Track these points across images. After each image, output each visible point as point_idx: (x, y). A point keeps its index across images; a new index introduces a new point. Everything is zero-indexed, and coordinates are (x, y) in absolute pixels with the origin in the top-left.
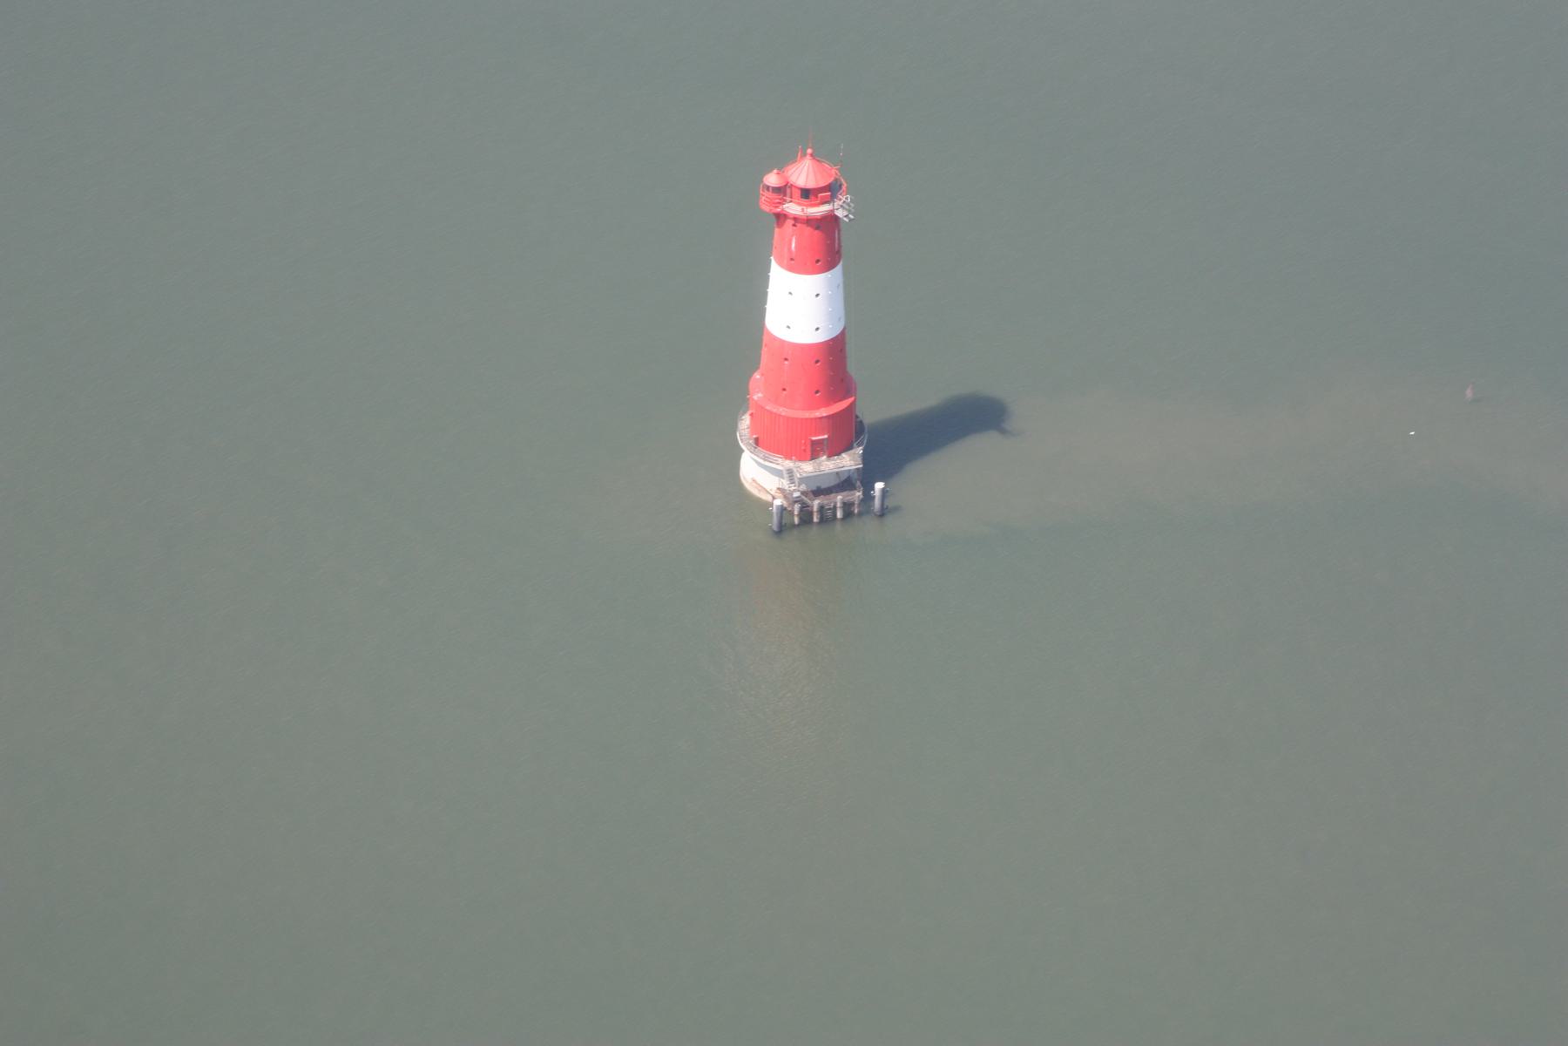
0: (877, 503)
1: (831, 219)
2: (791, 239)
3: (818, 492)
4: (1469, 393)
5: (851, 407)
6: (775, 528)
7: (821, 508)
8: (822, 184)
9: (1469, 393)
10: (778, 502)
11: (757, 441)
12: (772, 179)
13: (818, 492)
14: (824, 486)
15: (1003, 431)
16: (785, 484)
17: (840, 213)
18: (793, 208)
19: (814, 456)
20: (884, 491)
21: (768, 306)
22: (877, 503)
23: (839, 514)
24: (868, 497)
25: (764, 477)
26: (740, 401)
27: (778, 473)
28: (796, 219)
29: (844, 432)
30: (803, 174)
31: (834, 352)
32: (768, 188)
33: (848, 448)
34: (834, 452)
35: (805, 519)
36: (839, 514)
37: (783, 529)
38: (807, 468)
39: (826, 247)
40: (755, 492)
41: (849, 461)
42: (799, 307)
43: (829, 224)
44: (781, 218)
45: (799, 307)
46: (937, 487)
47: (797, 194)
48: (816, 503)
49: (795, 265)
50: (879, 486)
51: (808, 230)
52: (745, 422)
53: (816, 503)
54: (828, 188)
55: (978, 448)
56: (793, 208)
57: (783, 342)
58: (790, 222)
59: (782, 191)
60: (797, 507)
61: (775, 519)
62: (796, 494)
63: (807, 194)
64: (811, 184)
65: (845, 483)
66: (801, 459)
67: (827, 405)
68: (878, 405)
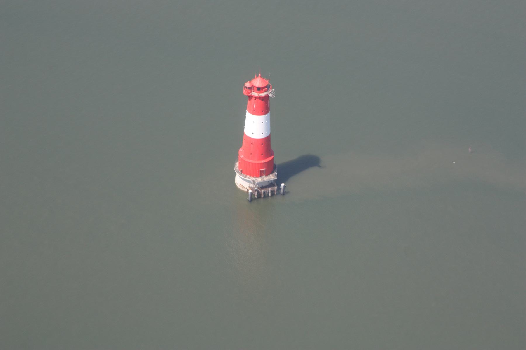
0: (282, 190)
1: (267, 97)
2: (254, 104)
3: (262, 188)
4: (470, 150)
7: (264, 193)
8: (264, 86)
9: (470, 150)
10: (250, 191)
11: (242, 171)
12: (248, 85)
13: (262, 188)
14: (264, 185)
15: (319, 166)
16: (252, 185)
17: (270, 95)
19: (261, 176)
20: (284, 187)
22: (282, 190)
23: (270, 195)
24: (279, 188)
25: (243, 183)
26: (236, 158)
27: (250, 182)
28: (256, 97)
29: (270, 168)
30: (258, 82)
31: (267, 141)
32: (246, 87)
33: (272, 172)
35: (258, 197)
36: (270, 195)
37: (252, 200)
38: (259, 180)
39: (265, 107)
40: (241, 188)
41: (272, 177)
42: (255, 126)
44: (250, 97)
45: (255, 126)
46: (301, 184)
47: (256, 89)
48: (263, 191)
49: (255, 112)
50: (283, 185)
51: (260, 101)
52: (237, 165)
53: (263, 191)
56: (255, 94)
57: (251, 138)
59: (251, 88)
60: (256, 193)
61: (249, 197)
62: (256, 188)
63: (259, 89)
64: (261, 86)
66: (257, 177)
67: (265, 158)
68: (278, 161)
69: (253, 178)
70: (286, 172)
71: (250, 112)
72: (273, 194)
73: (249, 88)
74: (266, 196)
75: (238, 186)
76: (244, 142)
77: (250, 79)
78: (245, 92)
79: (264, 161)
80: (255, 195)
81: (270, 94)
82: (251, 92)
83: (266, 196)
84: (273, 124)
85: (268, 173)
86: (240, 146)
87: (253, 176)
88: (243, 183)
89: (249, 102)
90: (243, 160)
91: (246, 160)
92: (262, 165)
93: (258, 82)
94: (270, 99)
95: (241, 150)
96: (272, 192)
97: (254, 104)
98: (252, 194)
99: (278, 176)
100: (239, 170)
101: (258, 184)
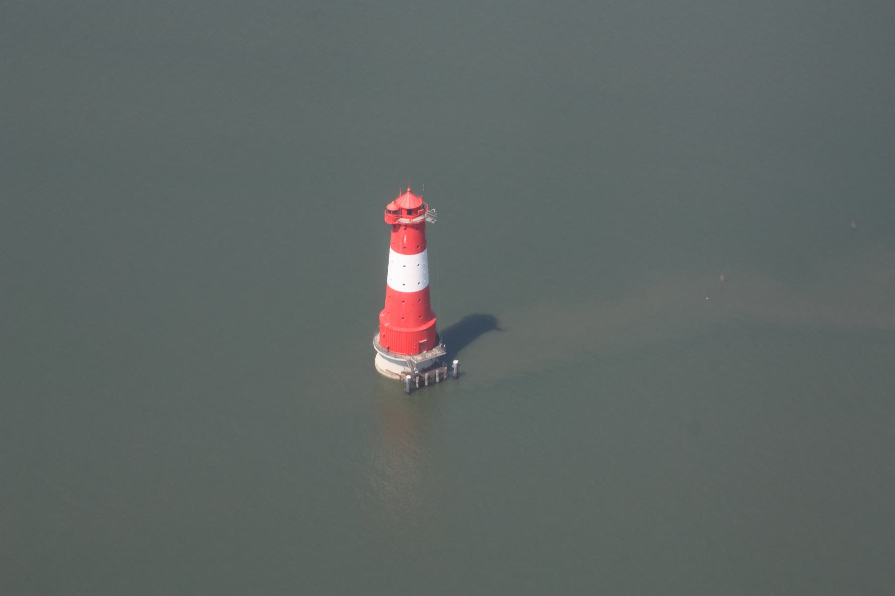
0: (455, 371)
1: (423, 223)
2: (404, 237)
3: (424, 370)
4: (722, 278)
5: (434, 326)
6: (407, 390)
7: (429, 378)
8: (417, 205)
9: (722, 278)
10: (409, 377)
11: (389, 348)
12: (392, 207)
13: (424, 370)
14: (425, 367)
15: (499, 330)
16: (409, 369)
17: (429, 219)
18: (404, 220)
19: (420, 352)
20: (458, 364)
21: (389, 276)
22: (455, 371)
23: (437, 380)
24: (450, 368)
25: (387, 365)
26: (374, 326)
27: (404, 364)
28: (406, 226)
29: (433, 338)
30: (407, 201)
31: (424, 296)
32: (390, 212)
33: (435, 345)
34: (429, 349)
35: (419, 386)
36: (437, 380)
37: (412, 390)
38: (418, 358)
39: (420, 239)
40: (389, 376)
41: (437, 352)
42: (405, 273)
43: (420, 227)
44: (396, 227)
45: (405, 273)
46: (479, 359)
47: (404, 212)
48: (426, 375)
49: (405, 250)
50: (456, 362)
51: (412, 231)
52: (378, 338)
53: (426, 375)
54: (422, 207)
55: (488, 338)
56: (404, 220)
57: (401, 293)
58: (402, 228)
59: (398, 212)
60: (417, 378)
61: (408, 386)
62: (417, 372)
63: (411, 212)
64: (412, 207)
65: (436, 363)
66: (416, 354)
67: (425, 323)
68: (443, 322)
70: (457, 337)
71: (397, 251)
72: (441, 380)
73: (395, 212)
74: (432, 382)
75: (384, 374)
76: (388, 302)
77: (394, 197)
78: (388, 219)
79: (424, 327)
80: (415, 383)
83: (432, 382)
84: (432, 269)
85: (429, 347)
87: (409, 355)
89: (393, 235)
90: (389, 330)
91: (395, 329)
92: (421, 334)
93: (407, 201)
94: (426, 226)
95: (382, 315)
96: (440, 374)
98: (411, 381)
99: (447, 350)
100: (384, 346)
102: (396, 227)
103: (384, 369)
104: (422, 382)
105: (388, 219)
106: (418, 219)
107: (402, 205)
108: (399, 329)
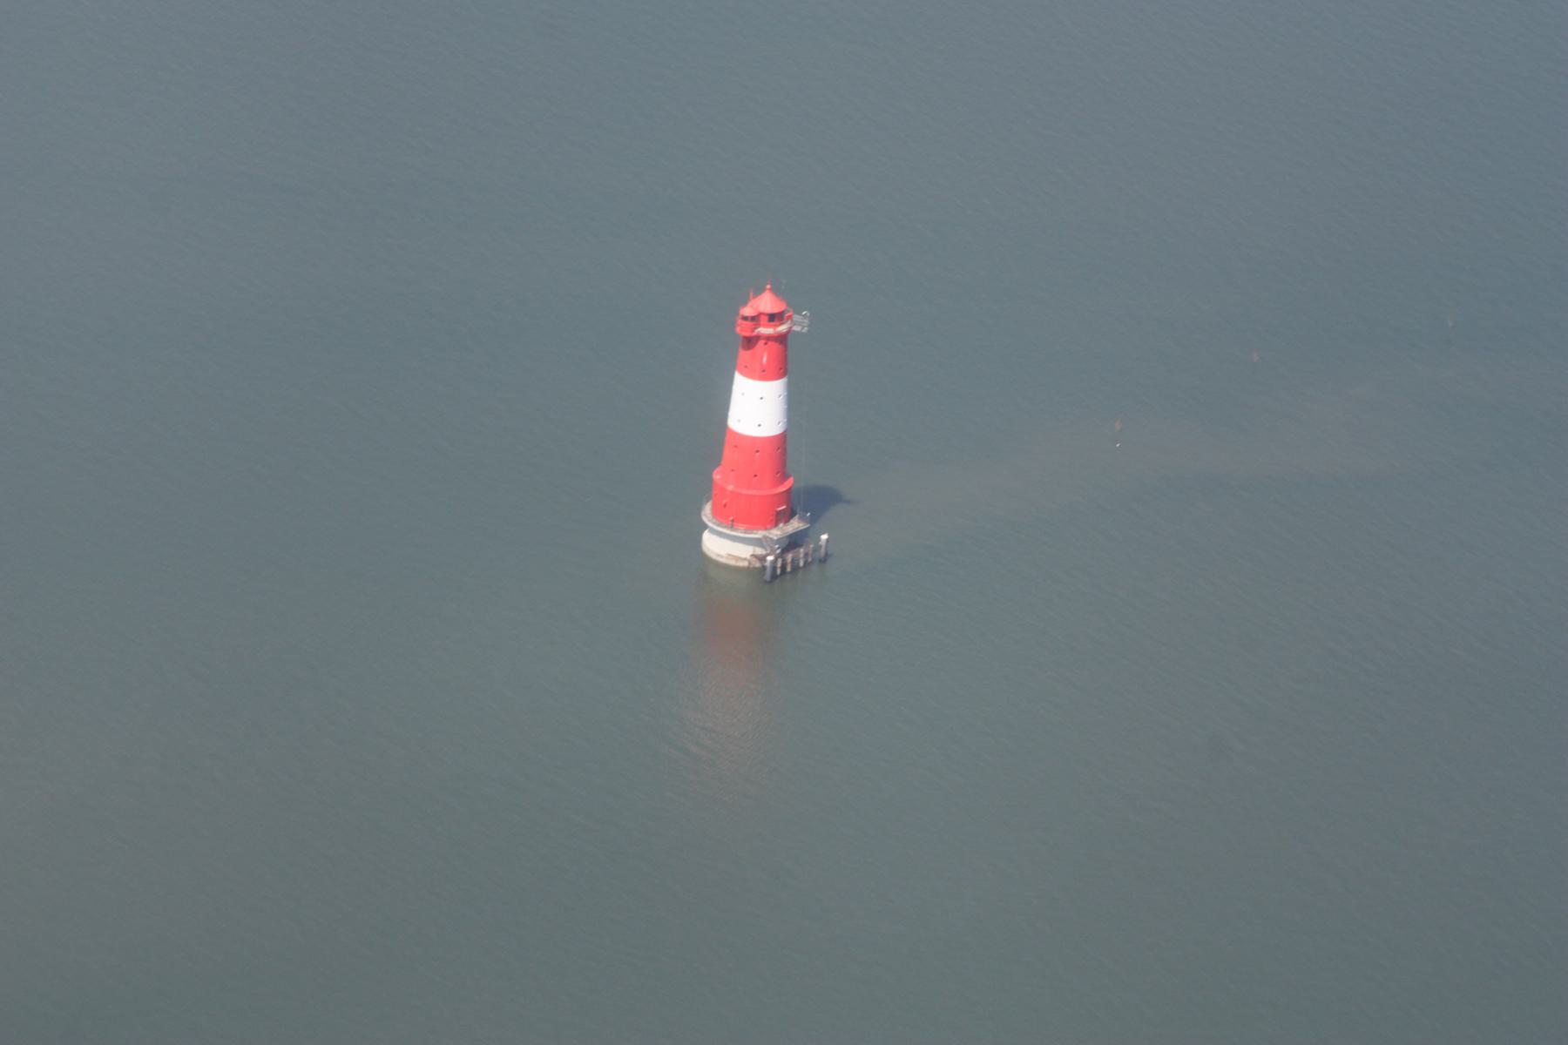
2: (764, 355)
12: (748, 311)
15: (848, 502)
16: (760, 551)
26: (705, 489)
27: (757, 542)
28: (769, 338)
30: (766, 303)
31: (781, 443)
32: (745, 318)
34: (787, 521)
35: (772, 579)
37: (774, 576)
38: (776, 533)
40: (732, 563)
42: (756, 407)
45: (756, 407)
47: (764, 320)
49: (765, 375)
51: (774, 346)
52: (707, 510)
53: (789, 557)
57: (754, 439)
58: (761, 343)
59: (756, 320)
63: (774, 318)
64: (776, 310)
65: (793, 542)
69: (759, 534)
73: (753, 318)
74: (796, 568)
76: (729, 454)
81: (797, 324)
82: (758, 325)
83: (796, 568)
84: (795, 405)
85: (788, 516)
86: (716, 459)
88: (725, 546)
91: (744, 492)
97: (764, 355)
101: (778, 541)
102: (750, 342)
103: (723, 553)
104: (784, 567)
105: (742, 330)
106: (783, 328)
107: (762, 309)
108: (750, 492)
